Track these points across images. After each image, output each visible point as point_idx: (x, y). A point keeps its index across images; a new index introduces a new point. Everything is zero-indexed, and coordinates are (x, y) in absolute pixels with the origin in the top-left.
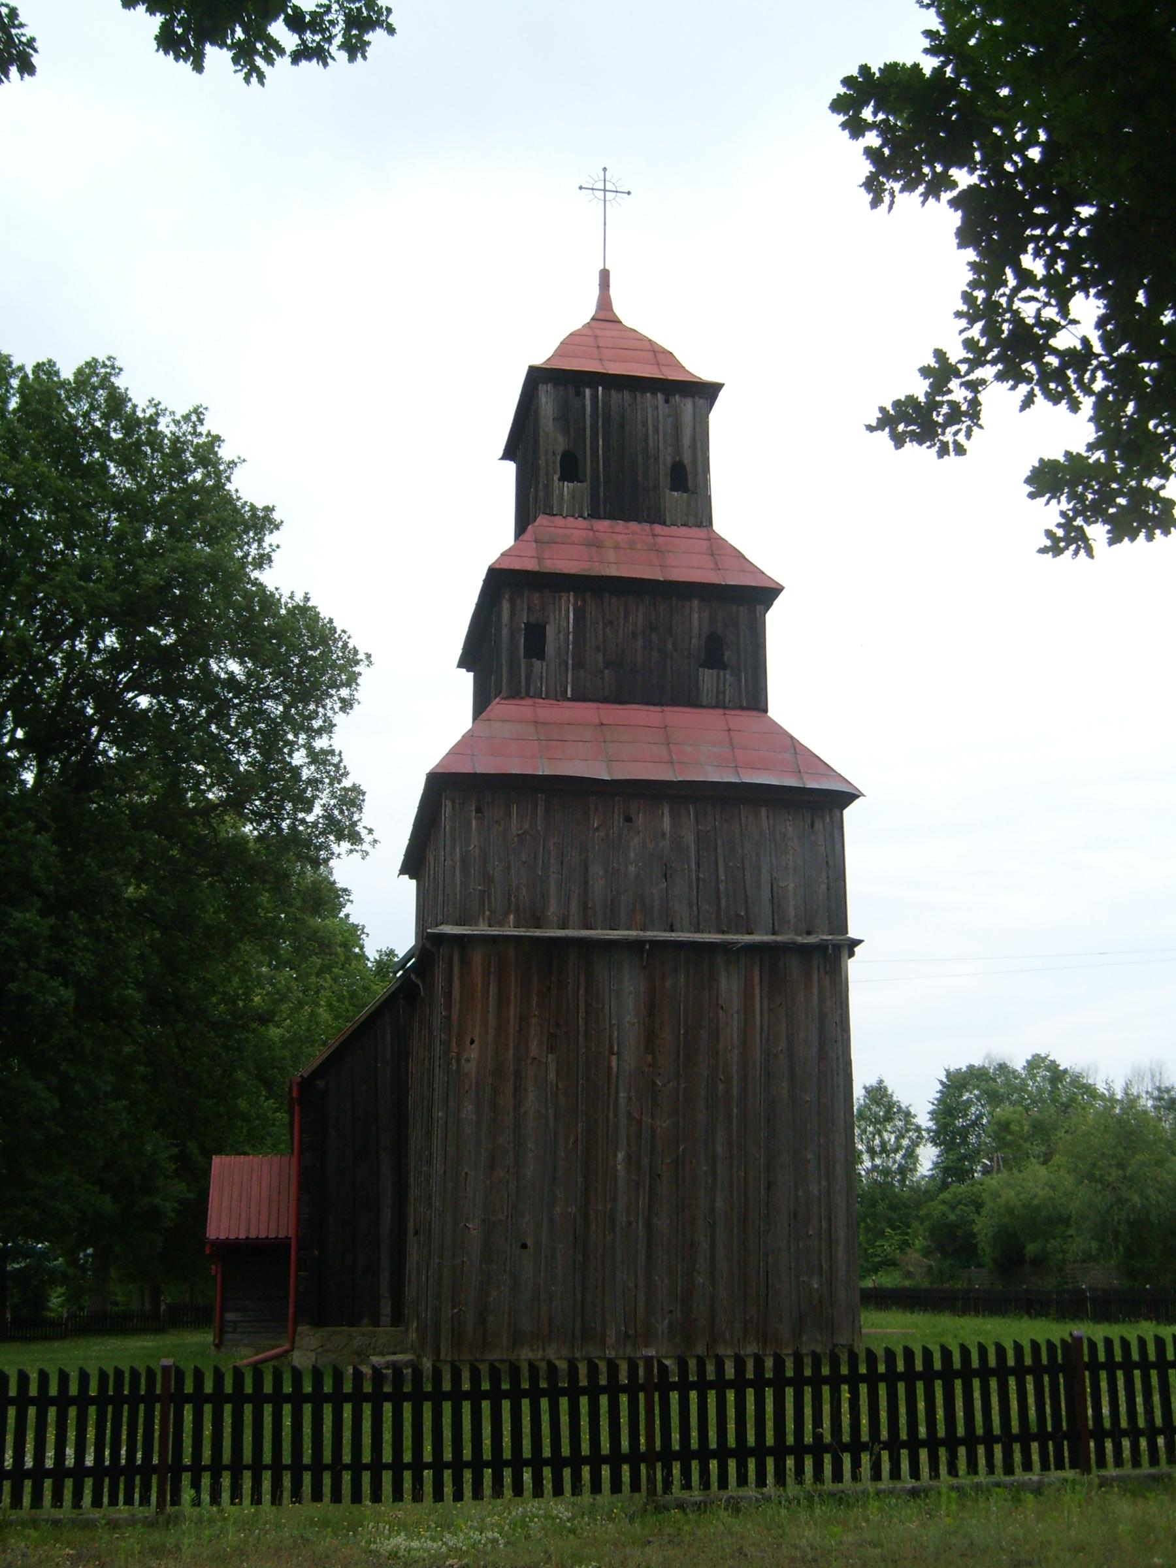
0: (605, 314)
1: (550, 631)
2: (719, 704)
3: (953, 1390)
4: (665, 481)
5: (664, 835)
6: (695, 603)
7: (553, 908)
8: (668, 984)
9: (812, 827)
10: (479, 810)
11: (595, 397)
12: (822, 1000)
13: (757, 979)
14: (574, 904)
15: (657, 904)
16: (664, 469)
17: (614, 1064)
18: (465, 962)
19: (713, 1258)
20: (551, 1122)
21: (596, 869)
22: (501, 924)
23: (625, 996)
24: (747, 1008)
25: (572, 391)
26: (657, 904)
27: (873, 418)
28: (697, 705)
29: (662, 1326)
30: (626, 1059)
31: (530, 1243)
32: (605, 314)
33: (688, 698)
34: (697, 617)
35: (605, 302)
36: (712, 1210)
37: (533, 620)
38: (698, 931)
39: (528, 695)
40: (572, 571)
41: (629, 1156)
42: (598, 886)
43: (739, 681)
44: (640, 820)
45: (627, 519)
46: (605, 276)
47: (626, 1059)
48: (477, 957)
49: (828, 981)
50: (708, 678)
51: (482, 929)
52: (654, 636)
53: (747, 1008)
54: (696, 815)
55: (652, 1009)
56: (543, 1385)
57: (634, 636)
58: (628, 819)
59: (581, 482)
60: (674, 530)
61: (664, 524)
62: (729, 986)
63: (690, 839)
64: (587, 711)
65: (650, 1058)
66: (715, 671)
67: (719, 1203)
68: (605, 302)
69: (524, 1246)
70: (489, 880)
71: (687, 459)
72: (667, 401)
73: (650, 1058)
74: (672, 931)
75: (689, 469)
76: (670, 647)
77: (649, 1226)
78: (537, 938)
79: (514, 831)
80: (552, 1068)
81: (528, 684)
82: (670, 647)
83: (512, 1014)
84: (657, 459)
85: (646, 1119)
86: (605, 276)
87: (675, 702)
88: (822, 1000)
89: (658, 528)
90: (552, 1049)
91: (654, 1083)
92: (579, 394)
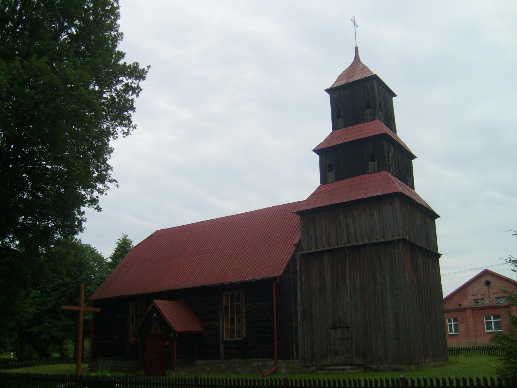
3: (386, 384)
35: (357, 57)
46: (356, 49)
60: (369, 123)
68: (357, 57)
86: (356, 49)
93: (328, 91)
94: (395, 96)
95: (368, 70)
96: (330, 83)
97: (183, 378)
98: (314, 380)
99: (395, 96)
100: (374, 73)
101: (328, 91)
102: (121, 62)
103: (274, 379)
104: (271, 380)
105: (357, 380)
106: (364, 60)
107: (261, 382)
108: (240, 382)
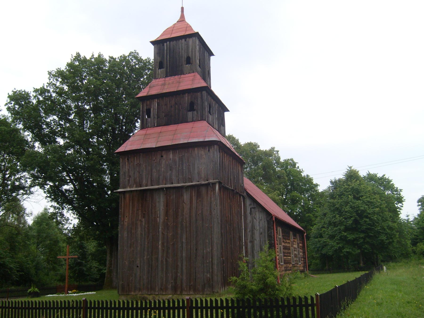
0: (182, 19)
1: (152, 110)
2: (193, 121)
3: (154, 304)
4: (184, 62)
5: (170, 159)
6: (187, 95)
7: (144, 182)
8: (171, 198)
9: (209, 151)
10: (128, 159)
11: (167, 45)
12: (211, 198)
13: (194, 194)
14: (149, 180)
15: (168, 178)
16: (184, 60)
17: (158, 220)
18: (125, 198)
19: (182, 269)
20: (143, 235)
21: (154, 170)
22: (132, 187)
23: (160, 202)
24: (191, 202)
25: (161, 45)
26: (168, 178)
27: (111, 56)
28: (187, 122)
29: (170, 286)
30: (161, 219)
31: (139, 266)
32: (182, 19)
33: (185, 121)
34: (187, 98)
35: (182, 16)
36: (182, 256)
37: (148, 108)
38: (179, 183)
39: (146, 128)
40: (154, 94)
41: (162, 243)
42: (155, 175)
43: (198, 113)
44: (165, 156)
45: (175, 75)
46: (182, 9)
47: (161, 219)
48: (127, 195)
49: (212, 193)
50: (190, 114)
51: (128, 189)
52: (177, 106)
53: (191, 202)
54: (179, 153)
55: (167, 205)
56: (303, 303)
57: (171, 107)
58: (162, 156)
59: (163, 68)
60: (187, 75)
61: (184, 74)
62: (186, 197)
63: (177, 159)
64: (159, 129)
65: (166, 218)
66: (192, 112)
67: (184, 255)
68: (182, 16)
69: (138, 267)
70: (130, 176)
71: (190, 55)
72: (185, 41)
73: (166, 218)
74: (172, 184)
75: (191, 58)
76: (180, 108)
77: (166, 261)
78: (141, 190)
79: (135, 164)
80: (144, 222)
81: (146, 125)
82: (180, 108)
83: (135, 209)
84: (182, 57)
85: (166, 234)
86: (182, 9)
87: (182, 122)
88: (211, 198)
89: (182, 76)
90: (144, 217)
91: (168, 224)
92: (163, 45)
93: (153, 43)
94: (228, 110)
95: (192, 29)
96: (156, 36)
97: (55, 301)
98: (42, 301)
99: (228, 110)
100: (196, 30)
101: (153, 43)
102: (239, 262)
103: (17, 302)
104: (211, 301)
105: (67, 302)
106: (188, 20)
107: (52, 304)
108: (109, 303)
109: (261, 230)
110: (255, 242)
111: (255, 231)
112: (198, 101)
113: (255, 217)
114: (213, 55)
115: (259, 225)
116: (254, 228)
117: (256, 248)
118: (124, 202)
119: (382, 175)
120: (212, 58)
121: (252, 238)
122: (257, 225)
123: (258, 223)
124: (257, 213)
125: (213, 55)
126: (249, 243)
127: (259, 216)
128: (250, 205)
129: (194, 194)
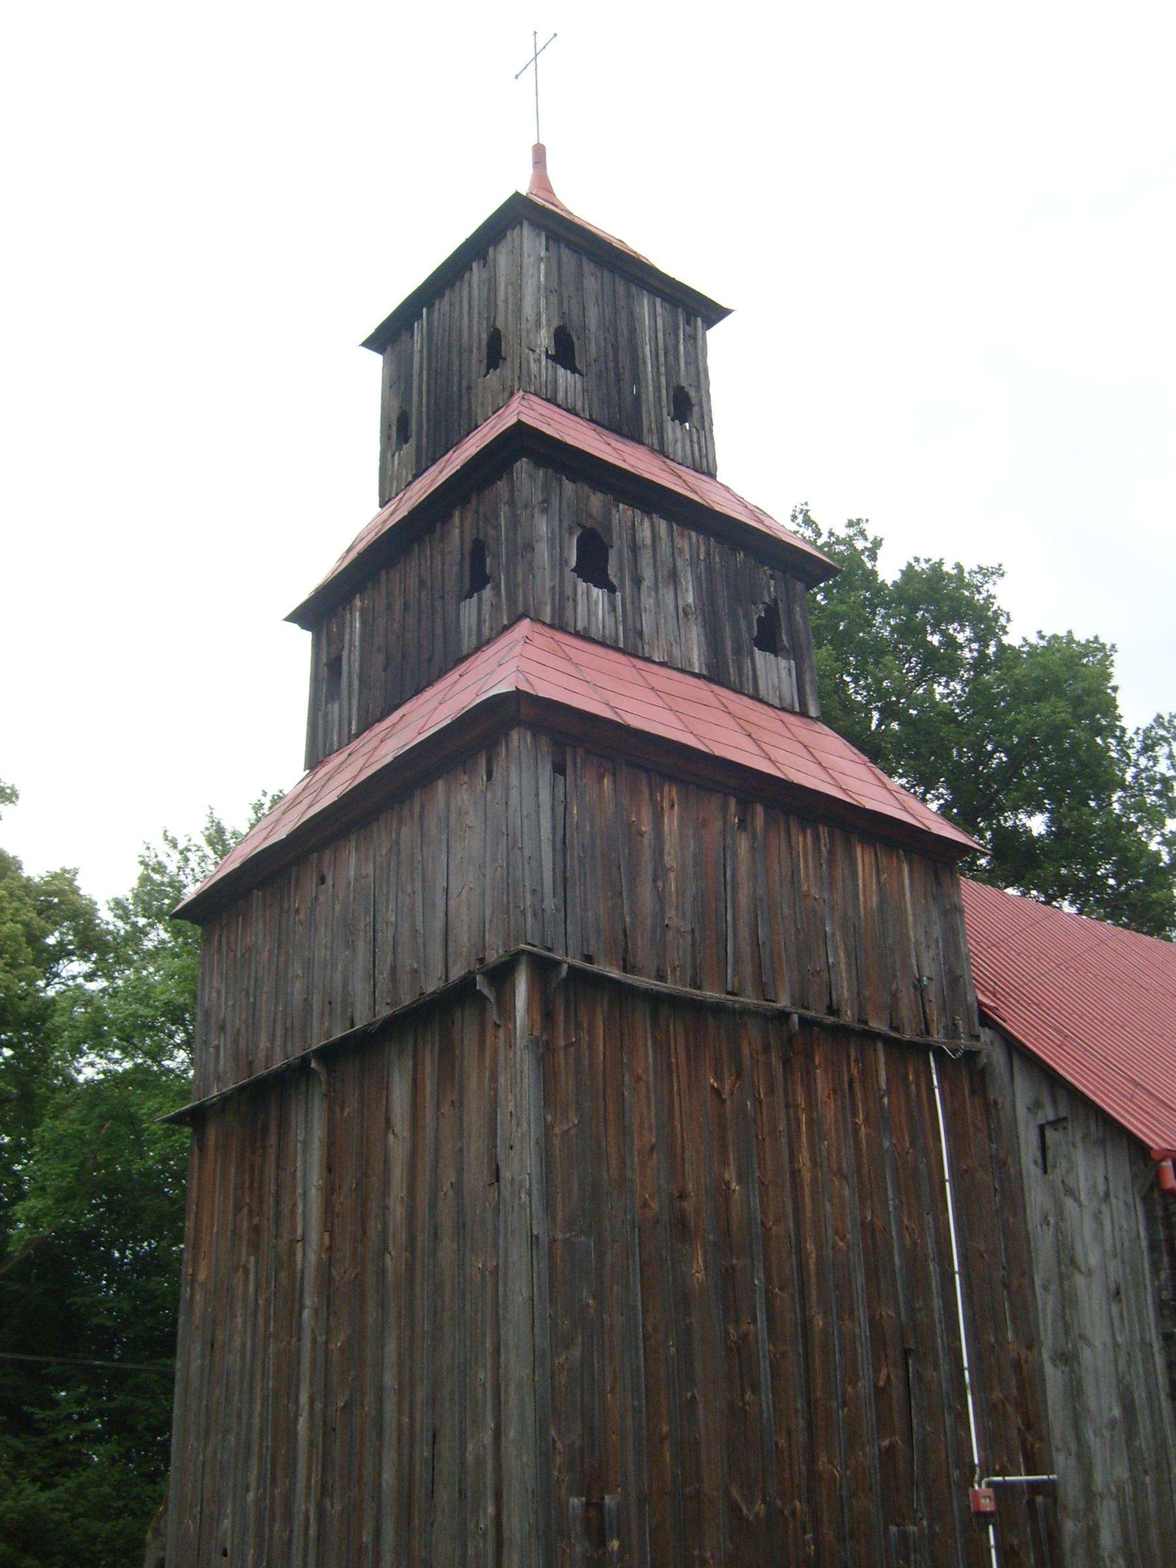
16: (478, 354)
30: (309, 1257)
46: (539, 153)
71: (500, 324)
86: (539, 153)
109: (1113, 1265)
110: (1086, 1354)
111: (1080, 1280)
112: (497, 527)
113: (1071, 1181)
114: (713, 313)
115: (1099, 1236)
116: (1073, 1262)
117: (1092, 1403)
118: (812, 1148)
119: (989, 563)
120: (716, 338)
121: (1067, 1333)
122: (1087, 1234)
123: (1088, 1225)
124: (1079, 1157)
125: (713, 313)
126: (1049, 1368)
127: (1087, 1169)
128: (1036, 1106)
129: (428, 1069)
